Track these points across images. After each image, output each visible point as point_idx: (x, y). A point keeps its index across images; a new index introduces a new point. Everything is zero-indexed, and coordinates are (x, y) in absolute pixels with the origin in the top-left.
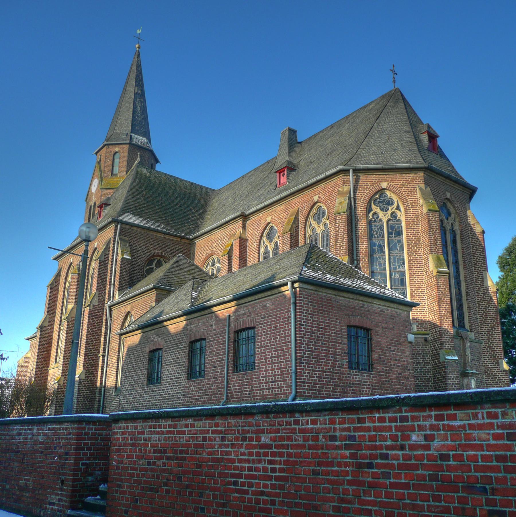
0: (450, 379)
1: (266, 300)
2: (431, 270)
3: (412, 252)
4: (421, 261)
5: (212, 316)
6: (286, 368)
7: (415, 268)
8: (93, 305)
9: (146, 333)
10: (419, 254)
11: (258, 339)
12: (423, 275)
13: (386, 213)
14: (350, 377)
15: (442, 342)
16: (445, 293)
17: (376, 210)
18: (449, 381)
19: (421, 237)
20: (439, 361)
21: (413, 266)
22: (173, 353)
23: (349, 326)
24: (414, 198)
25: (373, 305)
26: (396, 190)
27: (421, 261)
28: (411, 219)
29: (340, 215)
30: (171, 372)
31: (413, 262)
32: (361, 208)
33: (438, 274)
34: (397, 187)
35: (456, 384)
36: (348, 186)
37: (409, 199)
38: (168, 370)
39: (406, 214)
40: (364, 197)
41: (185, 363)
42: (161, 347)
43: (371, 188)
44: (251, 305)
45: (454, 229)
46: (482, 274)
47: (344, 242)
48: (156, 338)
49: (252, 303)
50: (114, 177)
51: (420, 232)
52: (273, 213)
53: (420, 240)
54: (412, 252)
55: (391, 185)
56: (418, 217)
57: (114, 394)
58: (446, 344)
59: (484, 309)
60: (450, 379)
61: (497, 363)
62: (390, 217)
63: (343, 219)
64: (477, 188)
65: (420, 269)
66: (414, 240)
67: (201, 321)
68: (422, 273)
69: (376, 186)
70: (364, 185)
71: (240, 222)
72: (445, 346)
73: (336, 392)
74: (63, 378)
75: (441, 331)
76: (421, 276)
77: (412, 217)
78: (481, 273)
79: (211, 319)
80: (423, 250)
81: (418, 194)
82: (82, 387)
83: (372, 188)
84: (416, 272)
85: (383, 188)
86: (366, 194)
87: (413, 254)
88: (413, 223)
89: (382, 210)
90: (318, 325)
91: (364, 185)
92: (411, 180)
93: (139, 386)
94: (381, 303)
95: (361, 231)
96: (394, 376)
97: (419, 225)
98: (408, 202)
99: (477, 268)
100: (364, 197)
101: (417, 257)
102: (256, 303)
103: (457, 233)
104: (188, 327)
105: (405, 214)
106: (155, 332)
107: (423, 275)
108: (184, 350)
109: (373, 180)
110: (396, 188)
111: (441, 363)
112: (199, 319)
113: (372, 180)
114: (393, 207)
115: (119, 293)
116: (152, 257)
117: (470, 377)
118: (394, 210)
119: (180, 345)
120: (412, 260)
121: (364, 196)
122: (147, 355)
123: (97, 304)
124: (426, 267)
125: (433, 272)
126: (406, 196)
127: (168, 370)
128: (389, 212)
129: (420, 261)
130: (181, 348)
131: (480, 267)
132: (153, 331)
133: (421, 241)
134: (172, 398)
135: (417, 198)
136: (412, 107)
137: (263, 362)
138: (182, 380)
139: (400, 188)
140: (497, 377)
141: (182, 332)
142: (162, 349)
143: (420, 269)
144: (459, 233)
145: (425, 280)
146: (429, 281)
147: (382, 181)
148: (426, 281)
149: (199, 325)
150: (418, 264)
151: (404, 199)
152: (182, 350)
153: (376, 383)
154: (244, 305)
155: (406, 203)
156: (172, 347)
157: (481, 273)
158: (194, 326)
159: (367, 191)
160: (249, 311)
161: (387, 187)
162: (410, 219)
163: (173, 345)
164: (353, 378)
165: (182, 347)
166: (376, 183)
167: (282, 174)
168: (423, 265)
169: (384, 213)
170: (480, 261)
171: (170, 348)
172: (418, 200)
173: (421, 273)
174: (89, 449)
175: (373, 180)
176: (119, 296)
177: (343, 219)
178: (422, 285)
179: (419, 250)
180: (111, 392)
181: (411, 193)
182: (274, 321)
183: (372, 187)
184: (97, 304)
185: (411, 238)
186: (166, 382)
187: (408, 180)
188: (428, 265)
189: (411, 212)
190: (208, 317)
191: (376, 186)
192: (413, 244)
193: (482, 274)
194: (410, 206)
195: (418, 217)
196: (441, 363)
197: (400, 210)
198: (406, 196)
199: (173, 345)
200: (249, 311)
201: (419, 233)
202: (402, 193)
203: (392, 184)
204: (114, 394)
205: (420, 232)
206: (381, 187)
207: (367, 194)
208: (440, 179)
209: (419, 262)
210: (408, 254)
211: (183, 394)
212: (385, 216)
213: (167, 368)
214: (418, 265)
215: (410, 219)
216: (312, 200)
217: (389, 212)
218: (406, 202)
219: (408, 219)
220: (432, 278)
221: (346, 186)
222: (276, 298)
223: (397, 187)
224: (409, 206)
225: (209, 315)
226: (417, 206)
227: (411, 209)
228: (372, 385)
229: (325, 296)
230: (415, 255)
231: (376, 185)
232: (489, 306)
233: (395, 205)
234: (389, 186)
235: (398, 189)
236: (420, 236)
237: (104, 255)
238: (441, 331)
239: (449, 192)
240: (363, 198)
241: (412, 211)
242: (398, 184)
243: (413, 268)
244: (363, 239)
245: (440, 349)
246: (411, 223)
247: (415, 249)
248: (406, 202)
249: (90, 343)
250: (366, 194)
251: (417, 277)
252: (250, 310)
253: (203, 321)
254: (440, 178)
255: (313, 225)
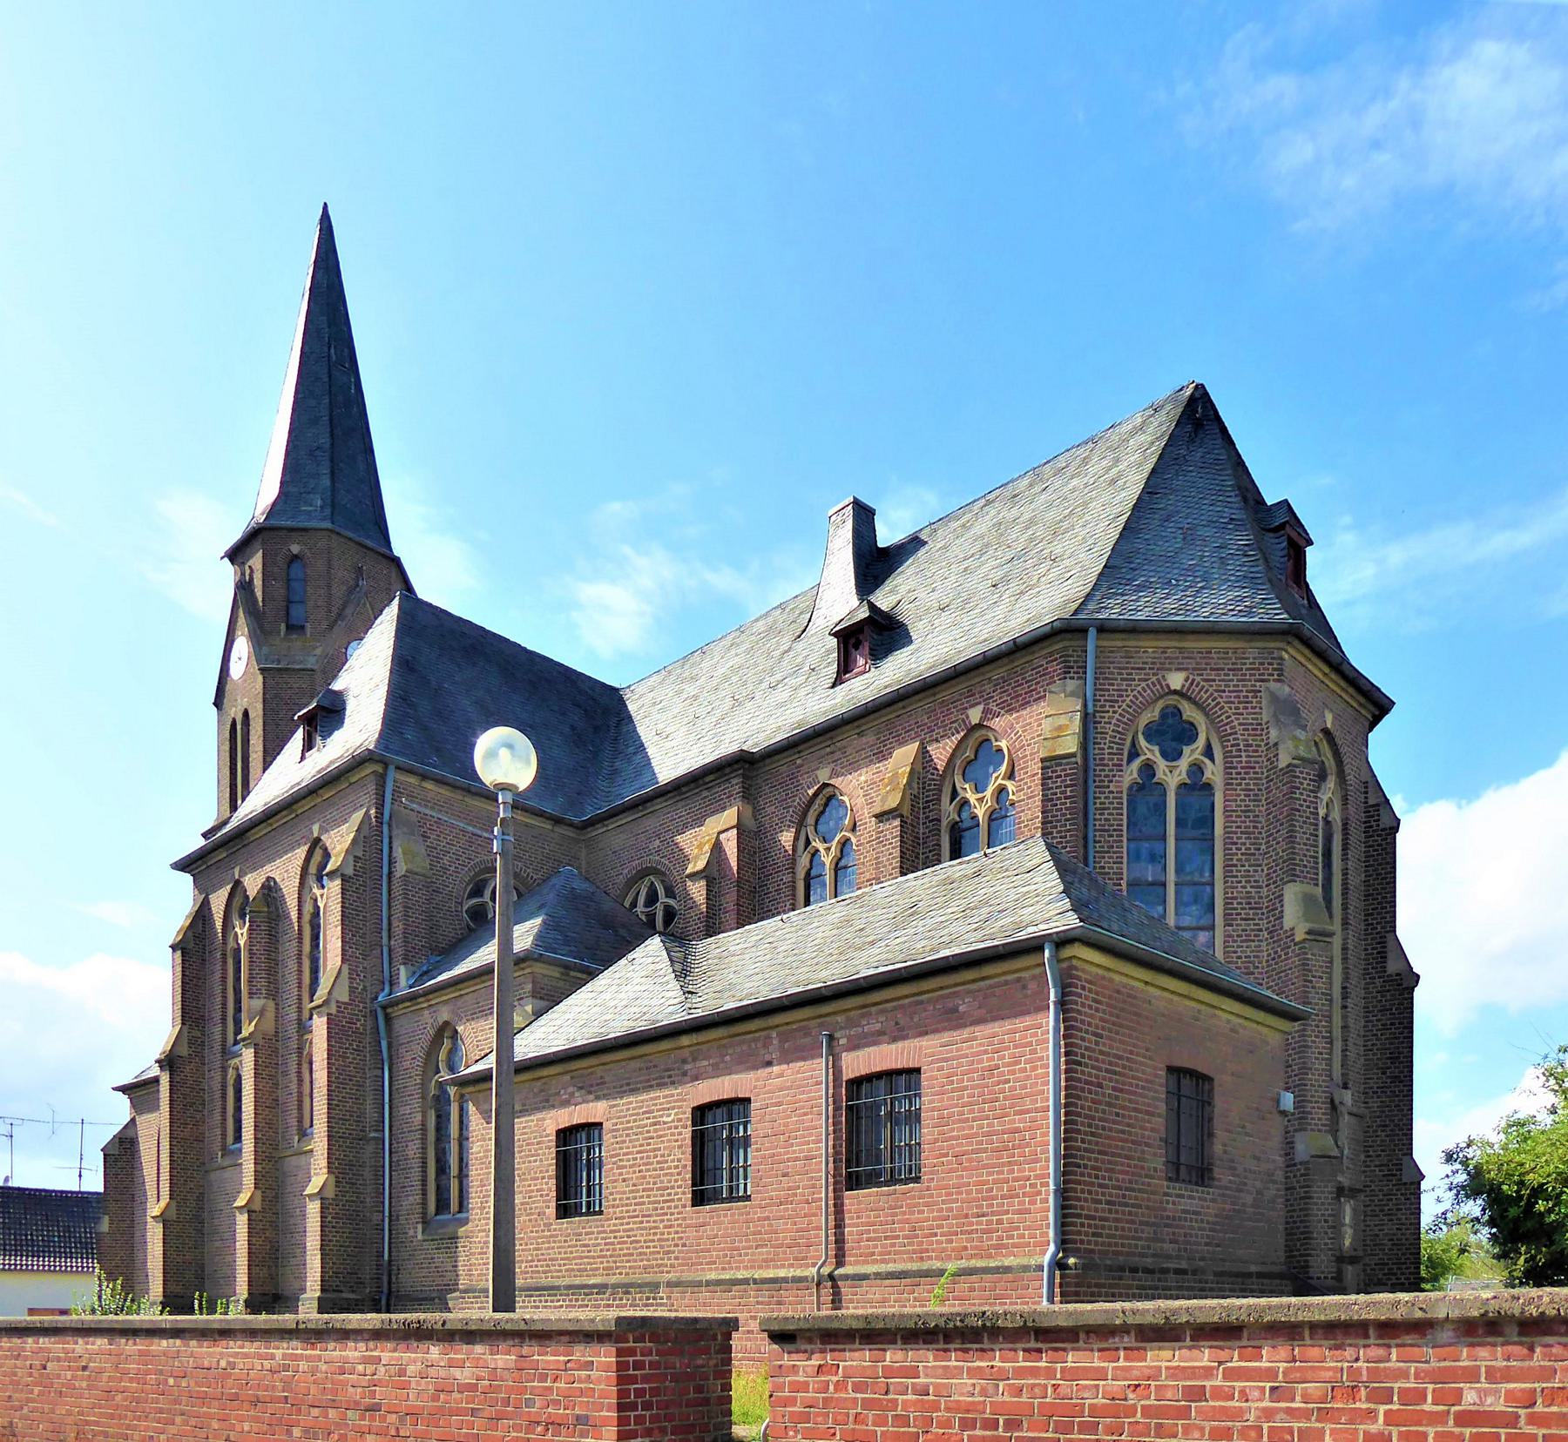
0: (1316, 1204)
1: (955, 993)
2: (1288, 922)
3: (1237, 876)
4: (1259, 903)
5: (769, 1037)
6: (1029, 1179)
7: (1241, 919)
8: (337, 1002)
9: (543, 1081)
10: (1255, 881)
11: (931, 1102)
12: (1261, 941)
13: (1174, 764)
14: (1168, 1202)
15: (1303, 1112)
16: (1319, 988)
17: (1149, 755)
18: (1313, 1210)
19: (1264, 835)
20: (1293, 1159)
21: (1237, 914)
22: (640, 1136)
23: (1171, 1070)
24: (1252, 724)
25: (1217, 1012)
26: (1205, 696)
27: (1259, 903)
28: (1240, 784)
29: (1057, 765)
30: (634, 1185)
31: (1238, 903)
32: (1109, 748)
33: (1308, 937)
34: (1211, 689)
35: (1329, 1215)
36: (1079, 678)
37: (1240, 724)
38: (624, 1180)
39: (1228, 767)
40: (1120, 715)
41: (683, 1162)
42: (597, 1120)
43: (1139, 688)
44: (902, 1007)
45: (1330, 819)
46: (1385, 942)
47: (1066, 842)
48: (577, 1094)
49: (906, 1001)
50: (294, 636)
51: (1260, 822)
52: (838, 755)
53: (1261, 844)
54: (1237, 876)
55: (1193, 680)
56: (1260, 779)
57: (420, 1237)
58: (1312, 1119)
59: (1379, 1033)
60: (1316, 1204)
61: (1397, 1164)
62: (1184, 775)
63: (1066, 775)
64: (1394, 703)
65: (1255, 925)
66: (1245, 844)
67: (730, 1051)
68: (1259, 936)
69: (1153, 683)
70: (1122, 679)
71: (734, 781)
72: (1310, 1124)
73: (1140, 1239)
74: (259, 1193)
75: (1305, 1085)
76: (1257, 943)
77: (1245, 779)
78: (1381, 937)
79: (765, 1046)
80: (1266, 872)
81: (1264, 712)
82: (329, 1219)
83: (1143, 689)
84: (1243, 930)
85: (1172, 688)
86: (1124, 706)
87: (1240, 882)
88: (1245, 795)
89: (1165, 755)
90: (1110, 1064)
91: (1122, 679)
92: (1247, 669)
93: (530, 1220)
94: (1237, 1007)
95: (1109, 814)
96: (1249, 1199)
97: (1260, 801)
98: (1236, 733)
99: (1372, 924)
100: (1120, 715)
101: (1249, 889)
102: (921, 1002)
103: (1335, 828)
104: (687, 1067)
105: (1226, 768)
106: (572, 1078)
107: (1261, 941)
108: (676, 1127)
109: (1146, 663)
110: (1207, 691)
111: (1295, 1165)
112: (725, 1046)
113: (1143, 663)
114: (1194, 746)
115: (407, 970)
116: (476, 874)
117: (1342, 1199)
118: (1197, 755)
119: (662, 1116)
120: (1236, 898)
121: (1120, 711)
122: (549, 1141)
123: (346, 999)
124: (1272, 919)
125: (1296, 931)
126: (1233, 717)
127: (624, 1180)
128: (1183, 764)
129: (1255, 903)
130: (665, 1123)
131: (1380, 923)
132: (567, 1078)
133: (1263, 847)
134: (645, 1254)
135: (1261, 724)
136: (216, 684)
137: (949, 1163)
138: (676, 1207)
139: (1216, 691)
140: (1394, 1197)
141: (675, 1079)
142: (601, 1124)
143: (1255, 925)
144: (1340, 829)
145: (1265, 954)
146: (1280, 956)
147: (1170, 670)
148: (1269, 955)
149: (723, 1061)
150: (1250, 909)
151: (1227, 724)
152: (670, 1128)
153: (1216, 1216)
154: (880, 1007)
155: (1231, 738)
156: (635, 1121)
157: (1381, 937)
158: (705, 1063)
159: (1127, 696)
160: (897, 1023)
161: (1183, 686)
162: (1237, 785)
163: (638, 1114)
164: (1174, 1203)
165: (670, 1119)
166: (1153, 674)
167: (853, 641)
168: (1263, 914)
169: (1169, 764)
170: (1382, 908)
171: (628, 1122)
172: (1263, 730)
173: (1255, 936)
174: (647, 1406)
175: (1146, 663)
176: (408, 979)
177: (1066, 775)
178: (1258, 967)
179: (1257, 871)
180: (411, 1233)
181: (1247, 708)
182: (986, 1052)
183: (1144, 684)
184: (346, 999)
185: (1237, 838)
186: (622, 1212)
187: (1242, 669)
188: (1282, 911)
189: (1241, 762)
190: (755, 1040)
191: (1153, 683)
192: (1242, 854)
193: (1385, 942)
194: (1242, 747)
195: (1260, 779)
196: (1295, 1165)
197: (1212, 759)
198: (1233, 717)
199: (638, 1114)
200: (897, 1023)
201: (1260, 825)
202: (1223, 707)
203: (1198, 679)
204: (420, 1237)
205: (1260, 822)
206: (1168, 686)
207: (1128, 706)
208: (1316, 672)
209: (1254, 905)
210: (1226, 882)
211: (680, 1242)
212: (1171, 772)
213: (621, 1174)
214: (1251, 912)
215: (1237, 785)
216: (963, 720)
217: (1183, 764)
218: (1230, 734)
219: (1232, 784)
220: (1289, 947)
221: (1072, 678)
222: (991, 987)
223: (1211, 689)
224: (1239, 745)
225: (757, 1035)
226: (1260, 746)
227: (1243, 754)
228: (1208, 1223)
229: (1125, 986)
230: (1243, 883)
231: (1154, 679)
232: (1392, 1024)
233: (1201, 742)
234: (1187, 685)
235: (1212, 694)
236: (1260, 833)
237: (351, 859)
238: (1305, 1085)
239: (1331, 710)
240: (1117, 716)
241: (1244, 759)
242: (1214, 680)
243: (1236, 919)
244: (1112, 836)
245: (1296, 1131)
246: (1240, 795)
247: (1247, 868)
248: (1230, 734)
249: (338, 1106)
250: (1124, 706)
251: (1245, 944)
252: (902, 1022)
253: (738, 1049)
254: (1315, 665)
255: (962, 794)
